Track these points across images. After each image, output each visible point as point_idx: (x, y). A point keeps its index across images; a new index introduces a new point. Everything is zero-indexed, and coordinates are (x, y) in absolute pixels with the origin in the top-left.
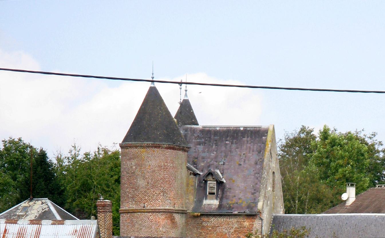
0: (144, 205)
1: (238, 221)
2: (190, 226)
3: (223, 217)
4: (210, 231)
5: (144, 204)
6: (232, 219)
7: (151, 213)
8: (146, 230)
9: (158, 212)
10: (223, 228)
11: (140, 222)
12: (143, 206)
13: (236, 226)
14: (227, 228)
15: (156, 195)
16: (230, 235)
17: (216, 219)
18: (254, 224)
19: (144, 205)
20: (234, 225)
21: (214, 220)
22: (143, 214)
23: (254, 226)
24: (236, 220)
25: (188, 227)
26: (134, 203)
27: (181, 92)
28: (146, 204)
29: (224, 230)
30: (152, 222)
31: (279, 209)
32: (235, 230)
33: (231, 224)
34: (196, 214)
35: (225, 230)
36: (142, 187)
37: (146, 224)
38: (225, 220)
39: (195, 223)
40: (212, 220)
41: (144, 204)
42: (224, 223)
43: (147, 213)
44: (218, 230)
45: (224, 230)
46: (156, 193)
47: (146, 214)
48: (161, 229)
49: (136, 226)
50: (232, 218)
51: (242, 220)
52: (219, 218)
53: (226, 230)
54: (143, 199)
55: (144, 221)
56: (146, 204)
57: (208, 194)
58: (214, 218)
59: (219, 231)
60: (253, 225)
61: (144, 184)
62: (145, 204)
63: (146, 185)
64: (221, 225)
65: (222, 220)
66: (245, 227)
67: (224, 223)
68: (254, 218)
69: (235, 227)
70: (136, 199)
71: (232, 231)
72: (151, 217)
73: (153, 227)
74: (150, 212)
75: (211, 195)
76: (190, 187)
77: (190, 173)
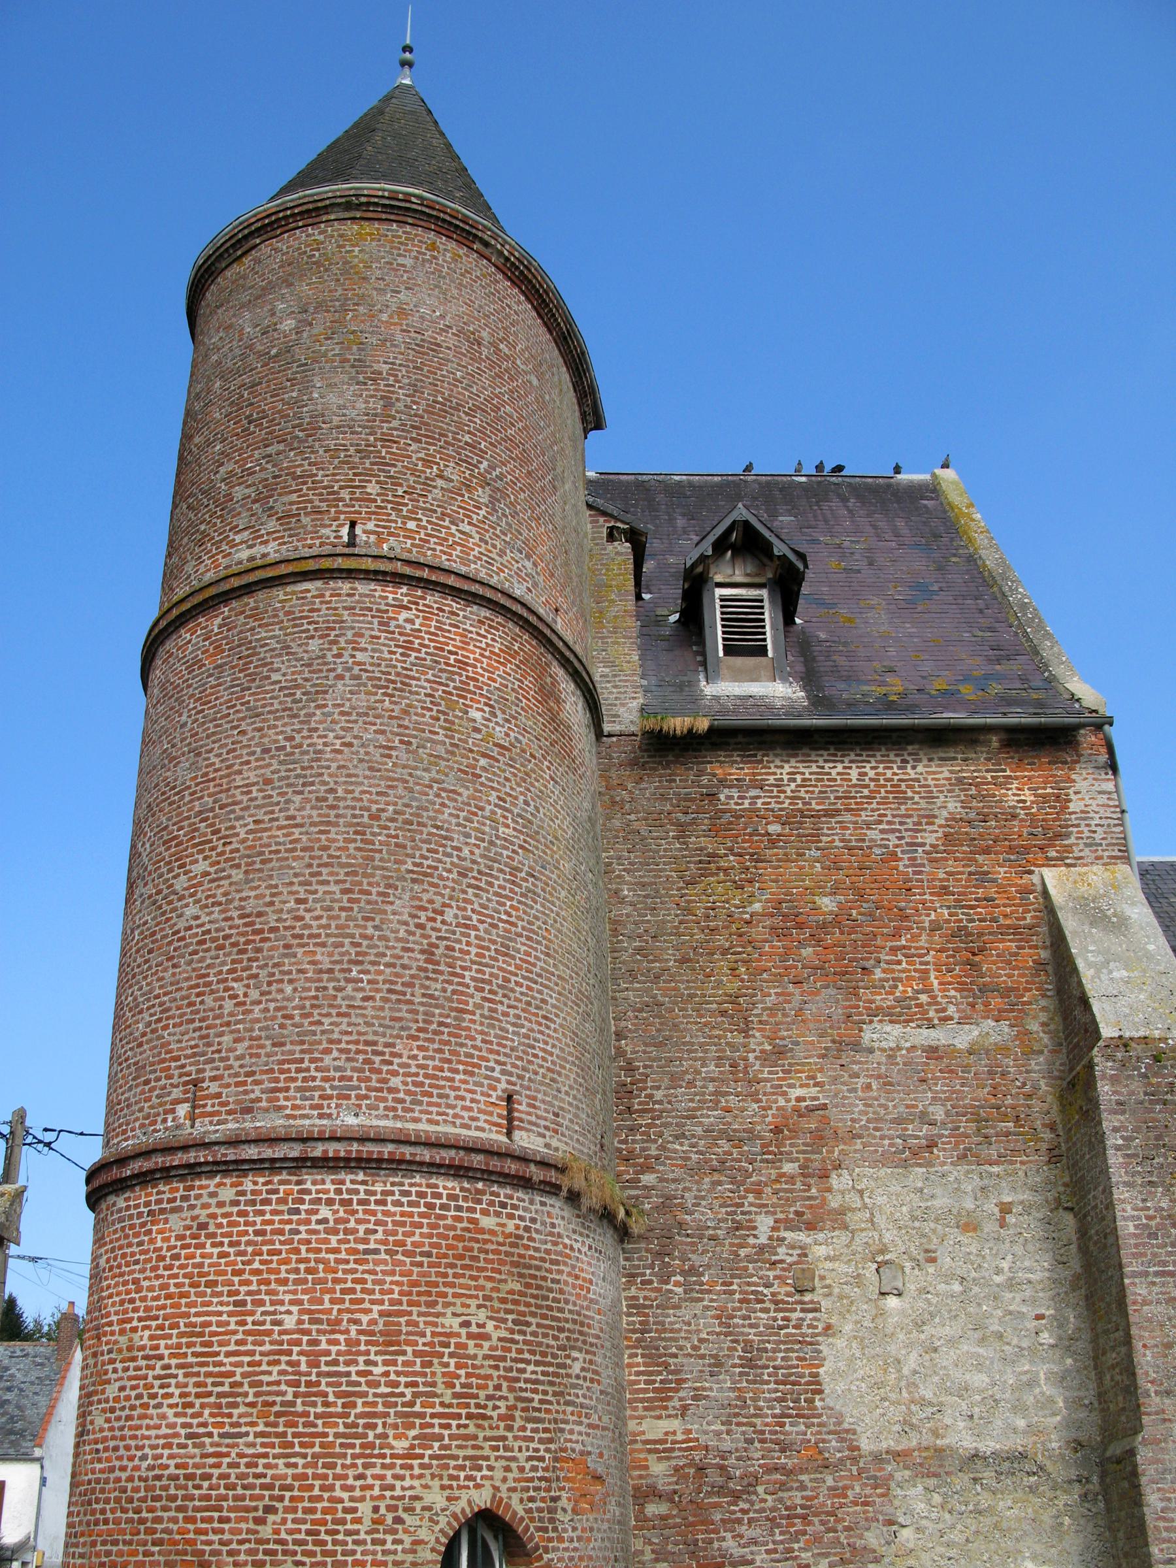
0: (352, 534)
1: (960, 781)
2: (633, 817)
3: (853, 757)
4: (773, 843)
5: (353, 525)
6: (920, 769)
7: (404, 590)
8: (361, 701)
9: (456, 593)
10: (868, 826)
11: (314, 645)
12: (346, 539)
13: (953, 806)
14: (889, 823)
15: (440, 483)
16: (923, 865)
17: (808, 771)
18: (1073, 797)
19: (352, 534)
20: (939, 802)
21: (799, 777)
22: (345, 586)
23: (1072, 807)
24: (947, 775)
25: (617, 823)
26: (272, 525)
27: (23, 1258)
28: (370, 526)
29: (873, 834)
30: (408, 647)
31: (1054, 882)
32: (946, 835)
33: (917, 798)
34: (678, 724)
35: (882, 831)
36: (338, 427)
37: (360, 656)
38: (872, 774)
39: (663, 797)
40: (786, 777)
41: (353, 525)
42: (866, 792)
43: (372, 586)
44: (833, 835)
45: (873, 834)
46: (441, 477)
47: (362, 588)
48: (477, 715)
49: (275, 677)
50: (930, 760)
51: (989, 775)
52: (826, 761)
53: (890, 836)
54: (345, 494)
55: (350, 634)
56: (370, 526)
57: (721, 654)
58: (793, 762)
59: (842, 841)
60: (1062, 801)
61: (361, 405)
62: (358, 530)
63: (372, 416)
64: (850, 803)
65: (854, 774)
66: (1014, 816)
67: (866, 792)
68: (1066, 763)
69: (945, 814)
70: (294, 497)
71: (931, 837)
72: (404, 615)
73: (422, 686)
74: (398, 579)
75: (739, 661)
76: (613, 601)
77: (611, 529)
